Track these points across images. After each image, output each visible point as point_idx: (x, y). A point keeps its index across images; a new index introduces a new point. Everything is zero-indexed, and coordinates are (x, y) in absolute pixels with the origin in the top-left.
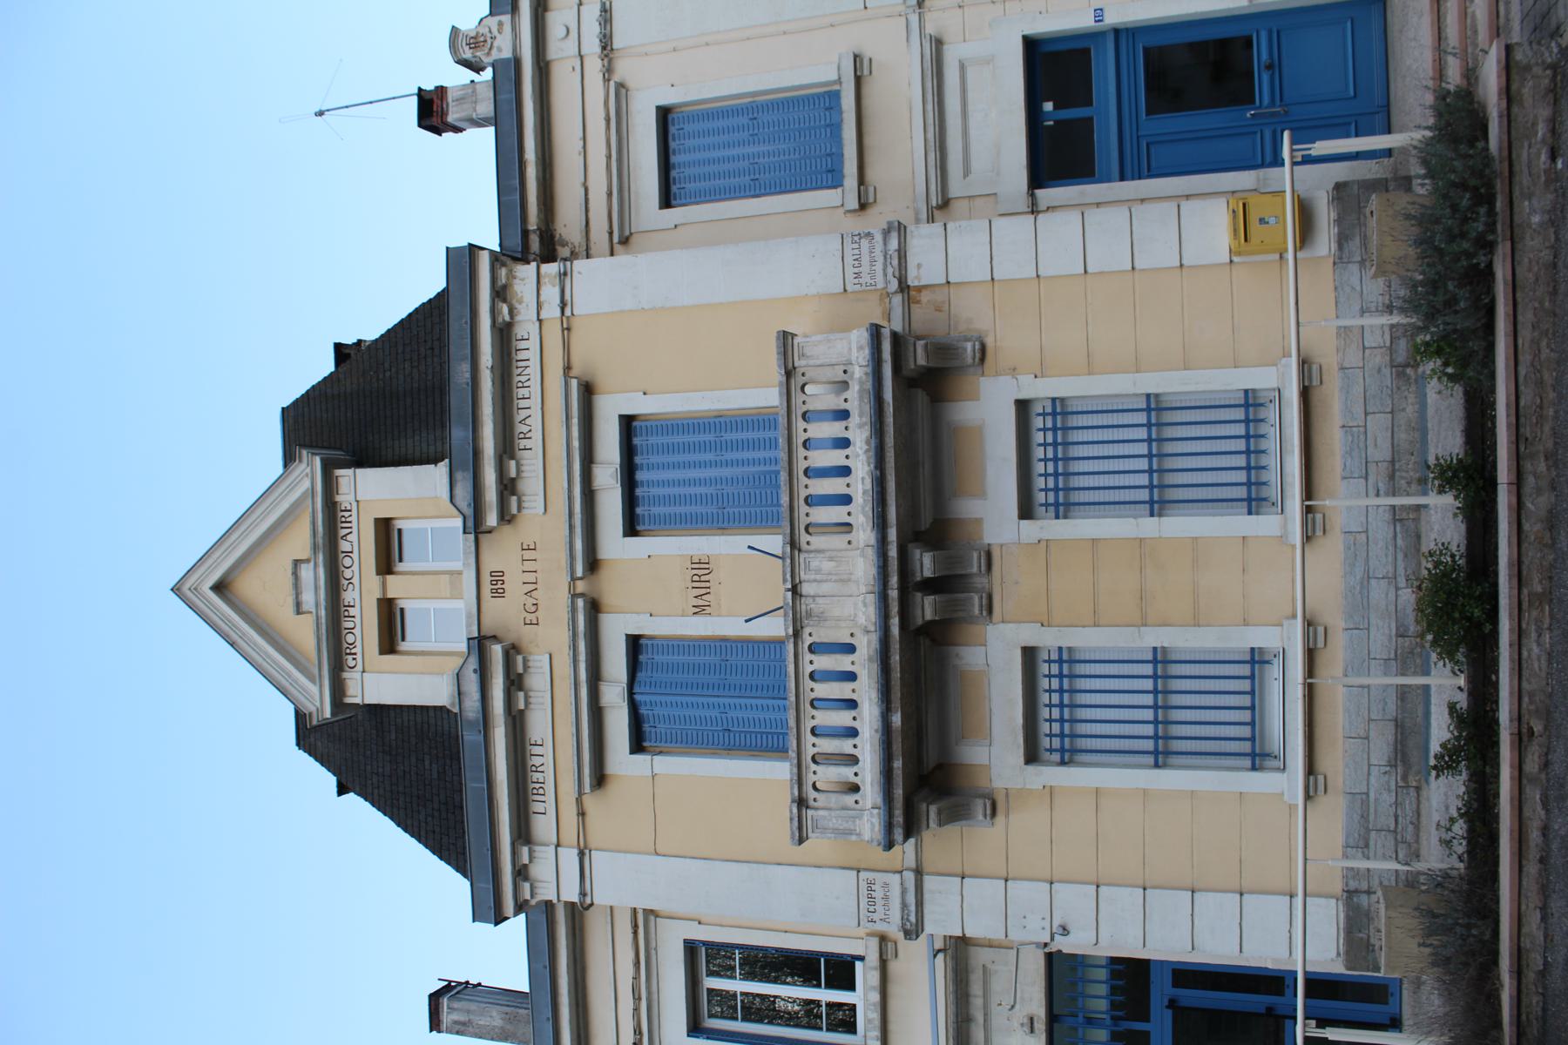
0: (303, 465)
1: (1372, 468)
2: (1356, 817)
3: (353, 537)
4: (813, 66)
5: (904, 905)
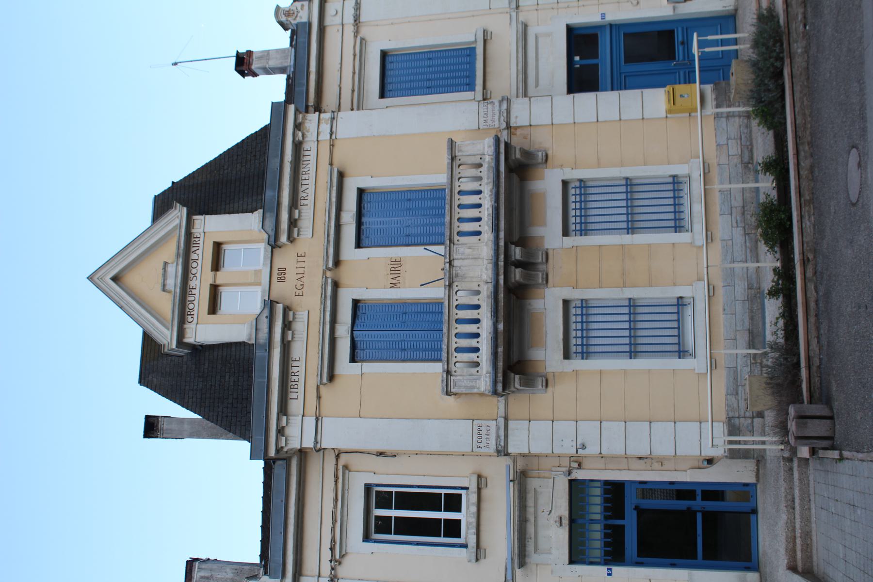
0: (177, 211)
1: (734, 210)
2: (732, 379)
3: (200, 252)
4: (460, 34)
5: (498, 436)
